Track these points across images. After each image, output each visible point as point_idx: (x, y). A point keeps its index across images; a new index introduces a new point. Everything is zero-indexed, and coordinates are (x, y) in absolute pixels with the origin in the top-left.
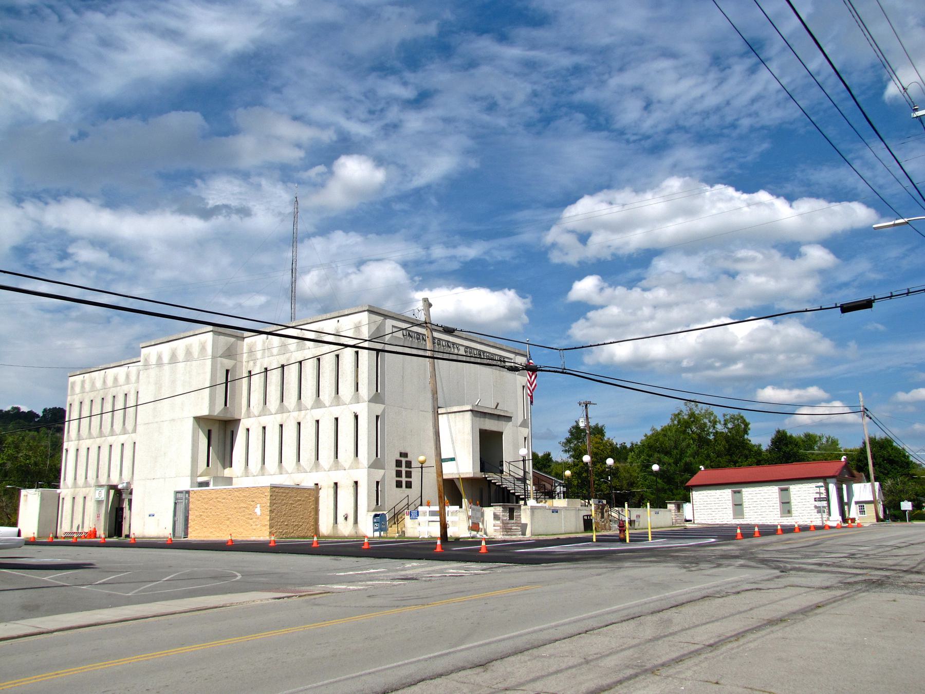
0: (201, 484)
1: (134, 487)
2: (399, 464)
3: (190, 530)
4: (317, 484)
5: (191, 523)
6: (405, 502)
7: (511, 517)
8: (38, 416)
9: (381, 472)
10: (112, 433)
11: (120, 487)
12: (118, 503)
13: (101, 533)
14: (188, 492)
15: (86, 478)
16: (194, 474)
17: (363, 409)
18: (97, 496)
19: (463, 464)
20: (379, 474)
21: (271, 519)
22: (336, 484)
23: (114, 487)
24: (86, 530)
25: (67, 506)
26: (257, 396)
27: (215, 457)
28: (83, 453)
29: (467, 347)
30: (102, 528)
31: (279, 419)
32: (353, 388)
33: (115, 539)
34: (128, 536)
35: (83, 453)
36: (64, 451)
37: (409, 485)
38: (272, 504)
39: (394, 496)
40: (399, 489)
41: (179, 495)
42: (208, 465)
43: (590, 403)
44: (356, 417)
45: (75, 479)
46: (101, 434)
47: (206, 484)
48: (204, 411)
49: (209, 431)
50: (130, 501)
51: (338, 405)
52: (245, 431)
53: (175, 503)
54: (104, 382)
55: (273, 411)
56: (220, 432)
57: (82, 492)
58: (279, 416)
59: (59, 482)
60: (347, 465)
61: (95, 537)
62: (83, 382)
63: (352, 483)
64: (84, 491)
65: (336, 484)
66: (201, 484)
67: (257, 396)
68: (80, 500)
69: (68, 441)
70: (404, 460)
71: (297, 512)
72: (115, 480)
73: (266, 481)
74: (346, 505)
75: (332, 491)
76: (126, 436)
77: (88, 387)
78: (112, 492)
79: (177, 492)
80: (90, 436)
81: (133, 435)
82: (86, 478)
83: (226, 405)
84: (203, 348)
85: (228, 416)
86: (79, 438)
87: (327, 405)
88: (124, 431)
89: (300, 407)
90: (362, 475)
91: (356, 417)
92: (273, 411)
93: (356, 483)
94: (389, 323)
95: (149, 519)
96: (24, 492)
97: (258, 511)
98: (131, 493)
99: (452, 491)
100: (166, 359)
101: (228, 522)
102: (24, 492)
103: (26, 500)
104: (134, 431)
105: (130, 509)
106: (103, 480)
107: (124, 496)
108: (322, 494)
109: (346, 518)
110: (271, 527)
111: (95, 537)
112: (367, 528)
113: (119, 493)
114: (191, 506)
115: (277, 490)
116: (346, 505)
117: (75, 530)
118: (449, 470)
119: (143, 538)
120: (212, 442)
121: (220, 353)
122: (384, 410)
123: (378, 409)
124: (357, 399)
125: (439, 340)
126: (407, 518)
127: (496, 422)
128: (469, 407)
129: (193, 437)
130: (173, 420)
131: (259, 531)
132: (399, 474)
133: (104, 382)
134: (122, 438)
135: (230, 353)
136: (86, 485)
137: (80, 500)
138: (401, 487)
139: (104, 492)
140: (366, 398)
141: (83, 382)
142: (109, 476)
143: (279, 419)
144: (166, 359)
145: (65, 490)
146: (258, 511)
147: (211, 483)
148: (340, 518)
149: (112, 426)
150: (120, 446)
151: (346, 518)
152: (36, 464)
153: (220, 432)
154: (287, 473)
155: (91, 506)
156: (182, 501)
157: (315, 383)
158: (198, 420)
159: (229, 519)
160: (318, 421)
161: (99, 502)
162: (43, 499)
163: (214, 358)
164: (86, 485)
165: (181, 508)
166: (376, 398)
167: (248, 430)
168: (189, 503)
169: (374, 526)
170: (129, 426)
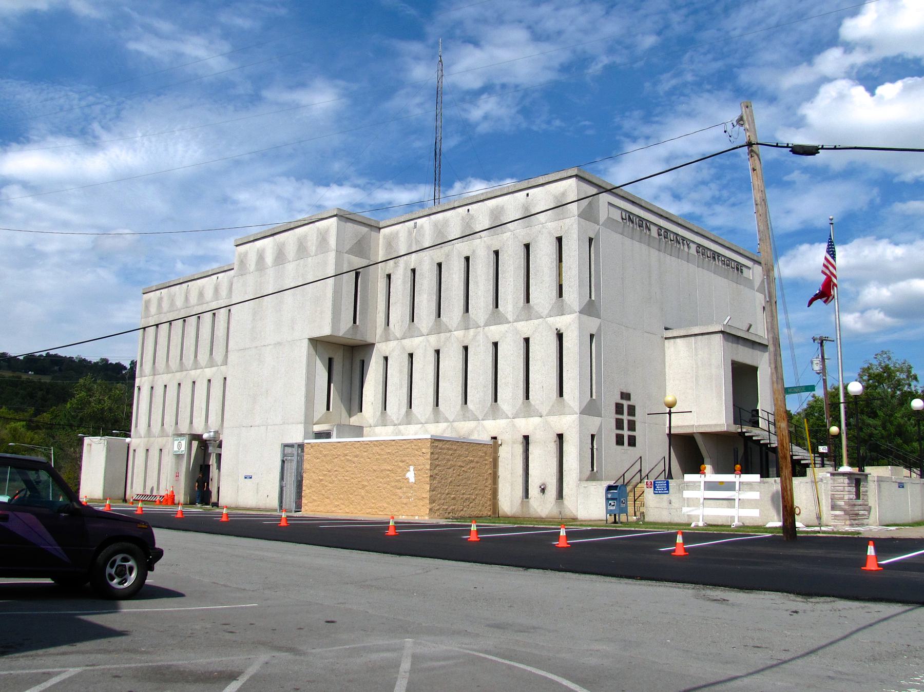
0: (319, 435)
1: (225, 438)
2: (619, 409)
3: (304, 501)
4: (495, 438)
5: (306, 491)
6: (637, 467)
7: (858, 496)
8: (125, 368)
9: (597, 421)
10: (196, 365)
11: (205, 436)
12: (204, 457)
13: (181, 497)
14: (301, 446)
15: (163, 425)
16: (308, 420)
17: (569, 323)
18: (176, 449)
19: (706, 409)
20: (594, 424)
21: (432, 490)
22: (526, 438)
23: (197, 437)
24: (163, 493)
25: (138, 461)
26: (399, 311)
27: (338, 398)
28: (159, 391)
29: (699, 246)
30: (182, 492)
31: (434, 341)
32: (555, 293)
33: (197, 509)
34: (216, 505)
35: (159, 391)
36: (136, 389)
37: (632, 442)
38: (433, 466)
39: (618, 461)
40: (620, 447)
41: (288, 450)
42: (328, 409)
43: (826, 339)
44: (560, 336)
45: (149, 426)
46: (182, 368)
47: (327, 435)
48: (325, 330)
49: (330, 360)
50: (219, 456)
51: (529, 318)
52: (382, 361)
53: (283, 462)
54: (187, 299)
55: (425, 331)
56: (345, 359)
57: (158, 442)
58: (433, 339)
59: (130, 431)
60: (544, 410)
61: (173, 503)
62: (160, 299)
63: (555, 438)
64: (161, 441)
65: (526, 438)
66: (319, 435)
67: (399, 311)
68: (154, 453)
69: (141, 376)
70: (625, 403)
71: (468, 478)
72: (198, 429)
73: (439, 430)
74: (542, 467)
75: (519, 449)
76: (214, 369)
77: (165, 305)
78: (195, 444)
79: (286, 446)
80: (168, 370)
81: (223, 368)
82: (163, 425)
83: (355, 322)
84: (323, 238)
85: (359, 338)
86: (154, 373)
87: (511, 319)
88: (211, 363)
89: (466, 324)
90: (569, 423)
91: (560, 336)
92: (425, 331)
93: (560, 437)
94: (605, 198)
95: (247, 483)
96: (87, 440)
97: (411, 475)
98: (220, 446)
99: (690, 451)
100: (269, 259)
101: (363, 492)
102: (87, 440)
103: (90, 451)
104: (225, 362)
105: (219, 467)
106: (184, 428)
107: (211, 449)
108: (503, 452)
109: (543, 491)
110: (432, 501)
111: (173, 503)
112: (589, 505)
113: (204, 444)
114: (306, 466)
115: (440, 445)
116: (542, 467)
117: (148, 493)
118: (682, 423)
119: (237, 508)
120: (335, 377)
121: (348, 247)
122: (600, 326)
123: (593, 324)
124: (560, 310)
125: (667, 231)
126: (649, 494)
127: (750, 350)
128: (719, 328)
129: (308, 365)
130: (279, 344)
131: (414, 509)
132: (619, 424)
133: (187, 299)
134: (209, 372)
135: (360, 248)
136: (163, 433)
137: (154, 453)
138: (623, 444)
139: (184, 443)
140: (576, 307)
141: (160, 299)
142: (191, 422)
143: (434, 341)
144: (269, 259)
145: (136, 441)
146: (411, 475)
147: (334, 434)
148: (534, 491)
149: (196, 356)
150: (206, 382)
151: (543, 491)
152: (110, 409)
153: (345, 359)
154: (447, 420)
155: (168, 461)
156: (293, 457)
157: (491, 287)
158: (316, 343)
159: (364, 486)
160: (496, 345)
161: (179, 456)
162: (109, 450)
163: (338, 252)
164: (163, 433)
165: (291, 467)
166: (590, 309)
167: (386, 359)
168: (302, 461)
169: (608, 504)
170: (218, 356)
